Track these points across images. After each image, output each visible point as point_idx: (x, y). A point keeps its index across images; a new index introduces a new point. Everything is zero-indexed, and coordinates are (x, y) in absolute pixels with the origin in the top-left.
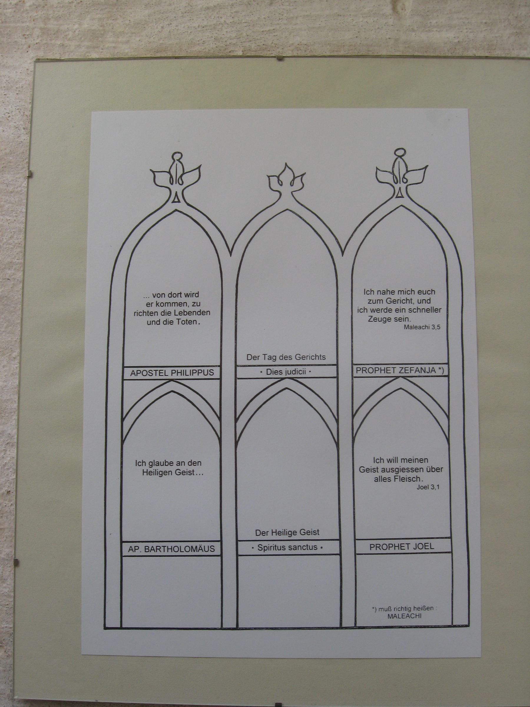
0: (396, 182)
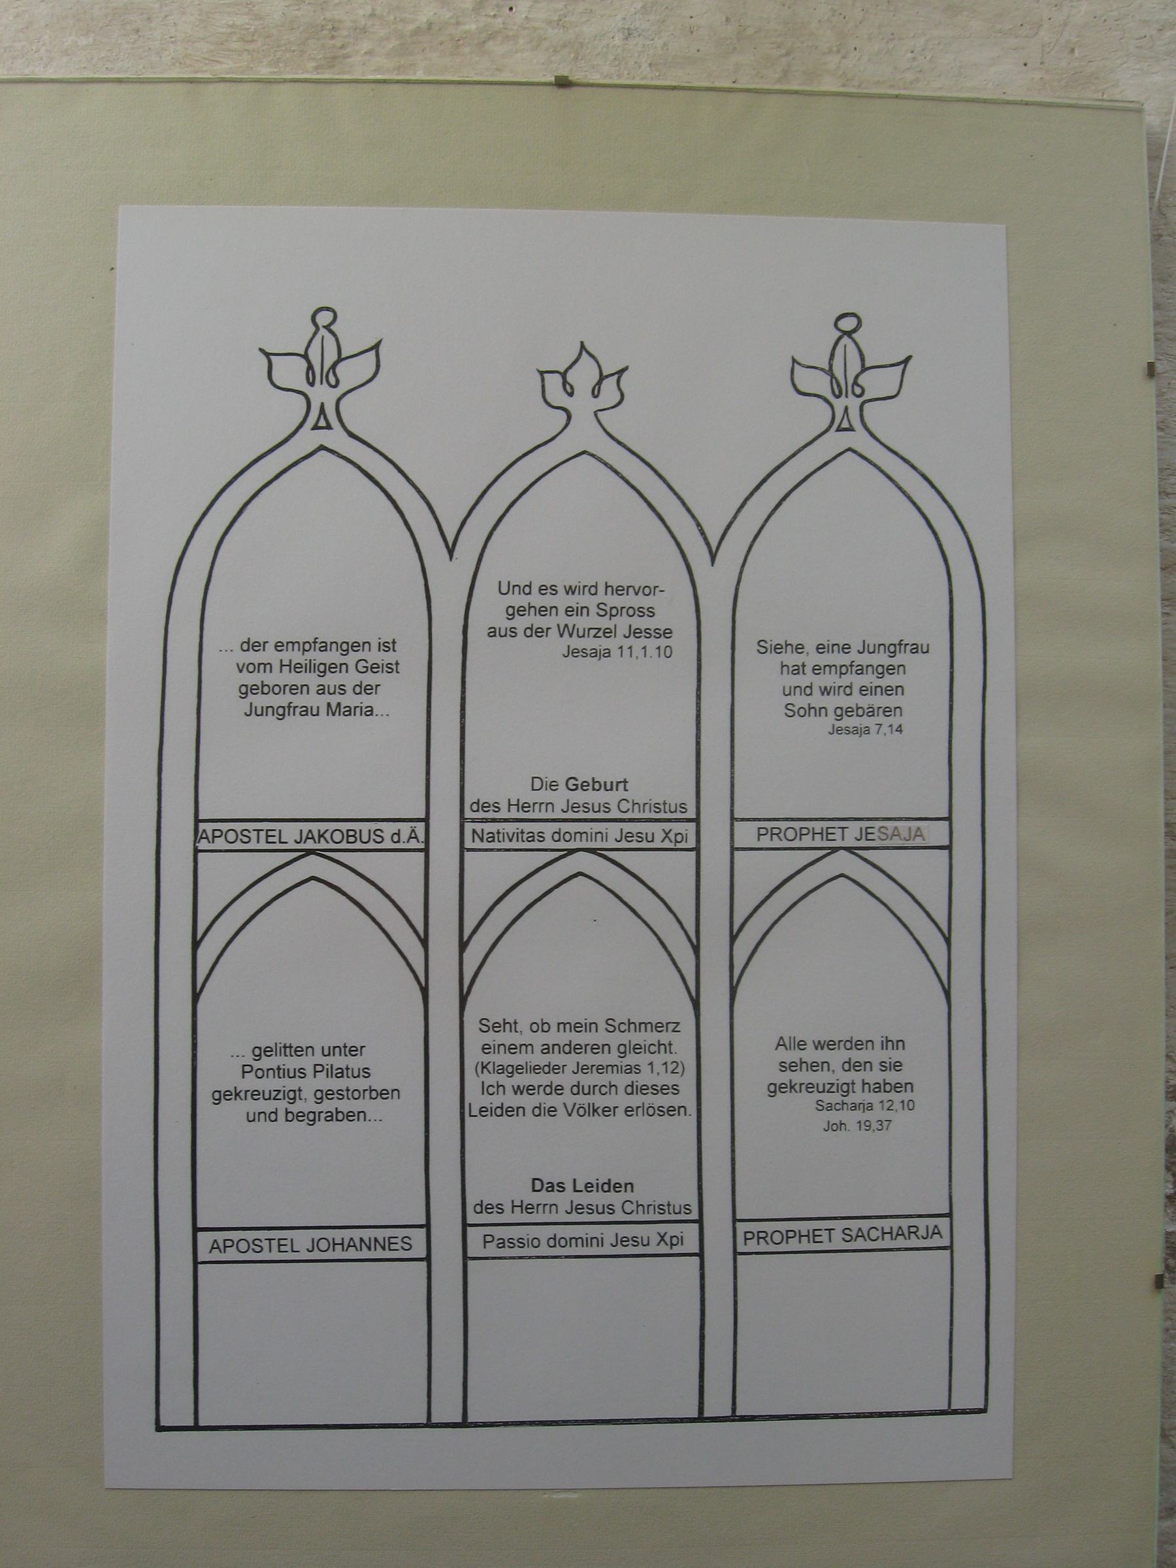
0: (837, 392)
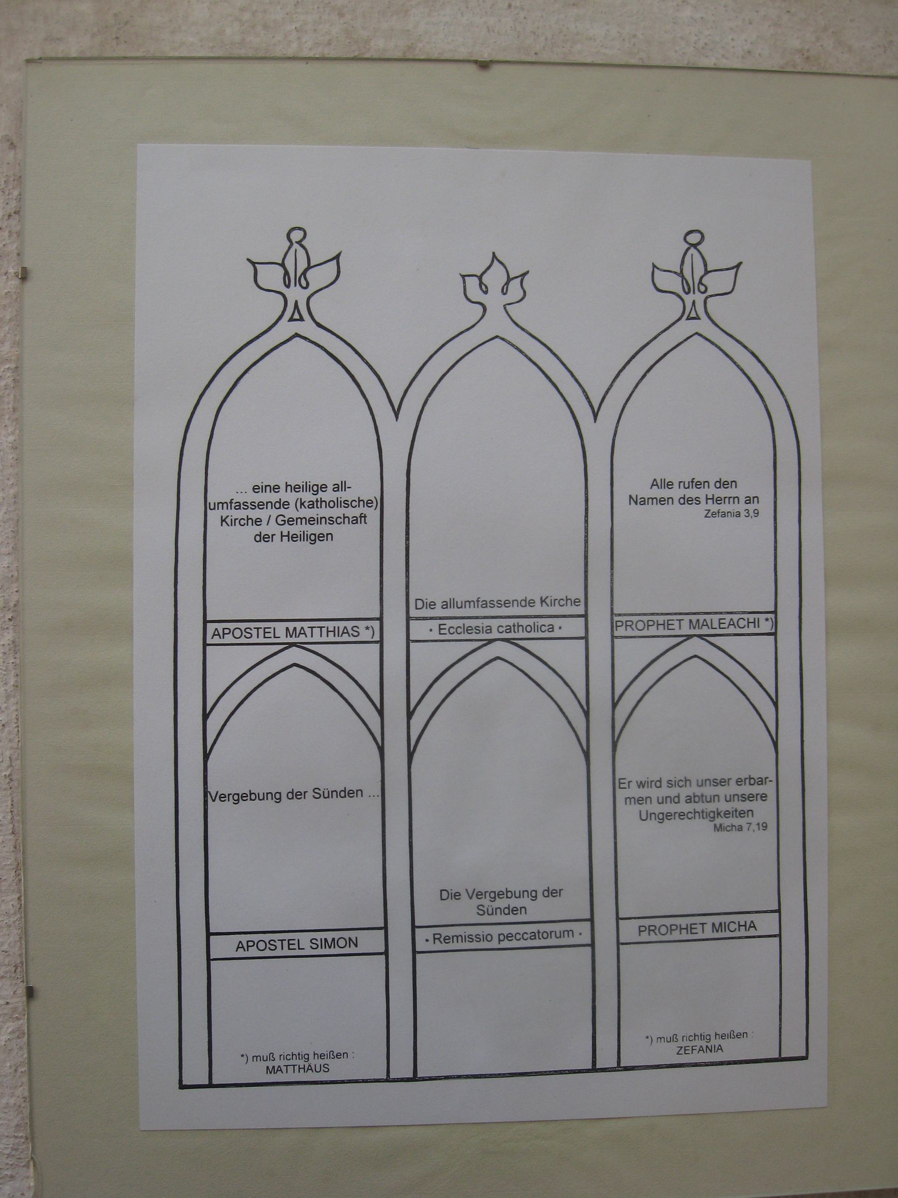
0: (687, 290)
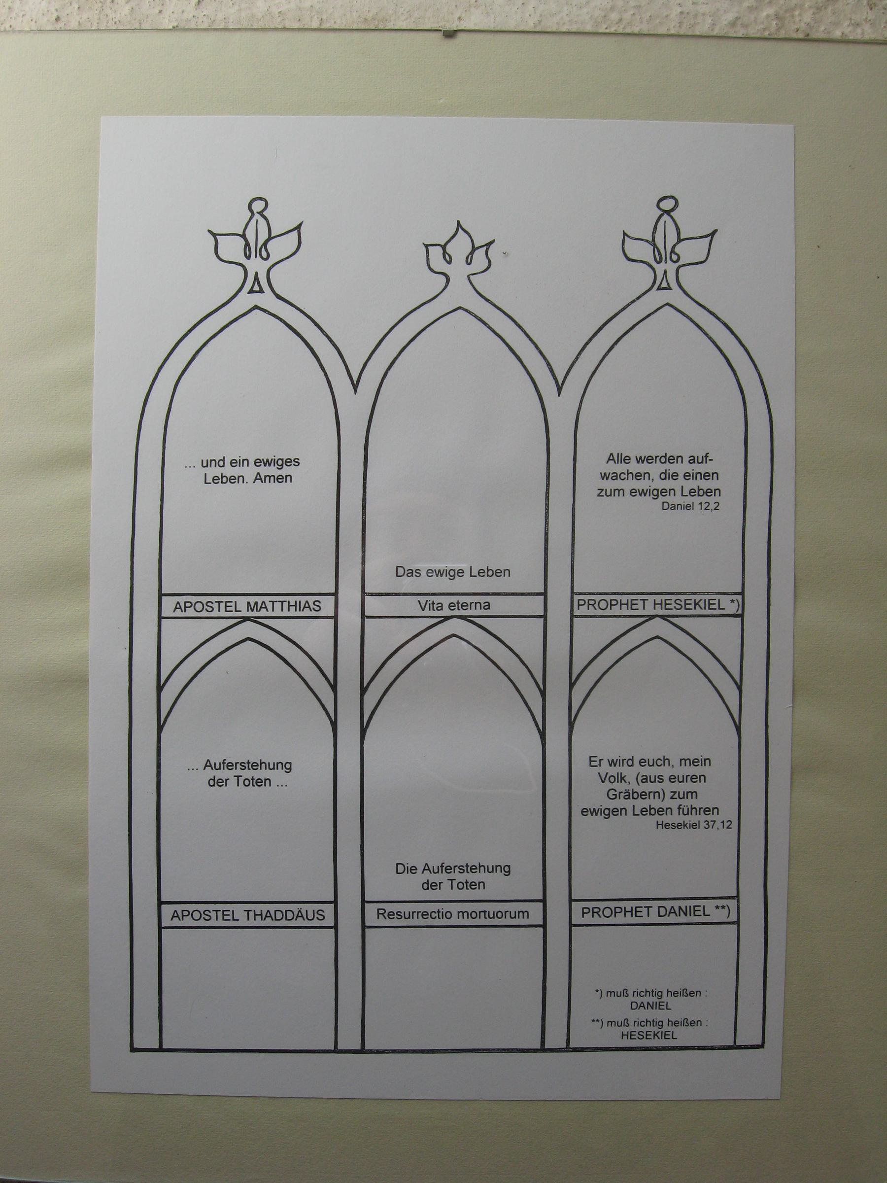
0: (658, 259)
